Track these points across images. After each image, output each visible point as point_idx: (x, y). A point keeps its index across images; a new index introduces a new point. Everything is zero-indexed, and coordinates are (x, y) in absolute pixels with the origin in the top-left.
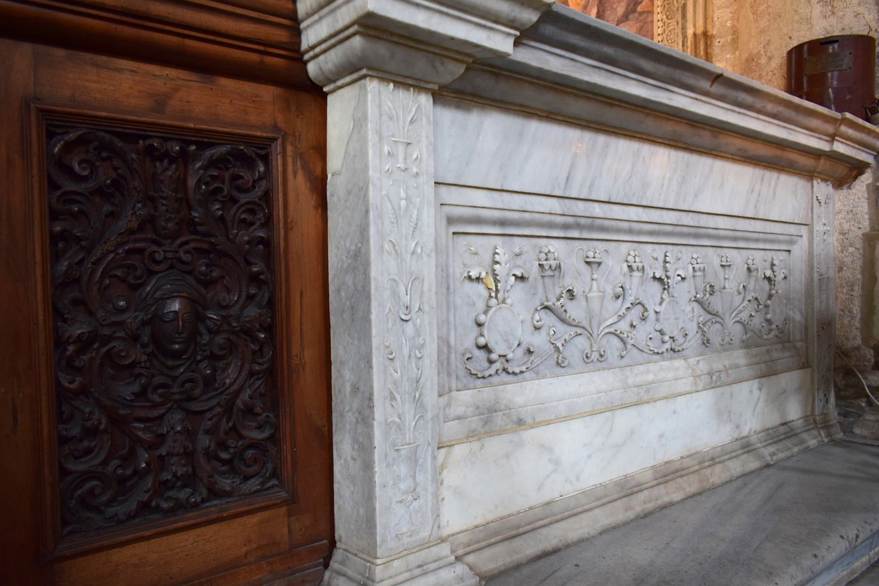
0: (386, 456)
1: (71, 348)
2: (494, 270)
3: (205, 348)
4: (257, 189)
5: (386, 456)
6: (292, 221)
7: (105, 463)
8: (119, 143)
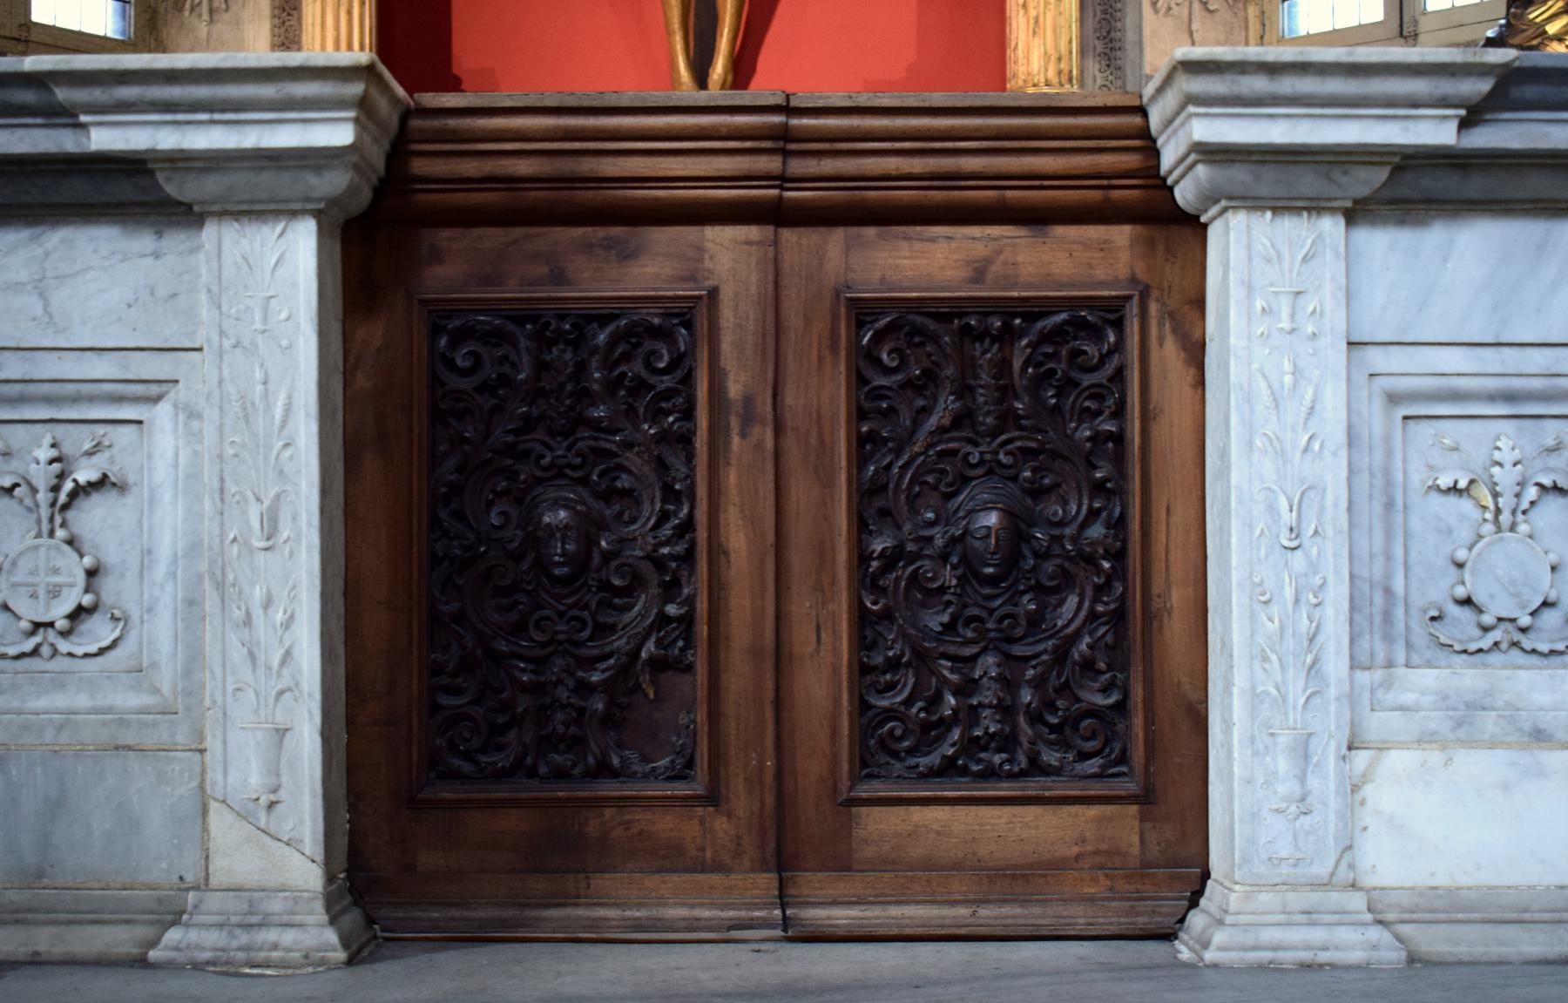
0: (1252, 740)
1: (875, 564)
2: (1492, 476)
3: (1028, 576)
4: (1107, 366)
5: (1252, 740)
6: (1155, 408)
7: (908, 702)
8: (931, 325)
